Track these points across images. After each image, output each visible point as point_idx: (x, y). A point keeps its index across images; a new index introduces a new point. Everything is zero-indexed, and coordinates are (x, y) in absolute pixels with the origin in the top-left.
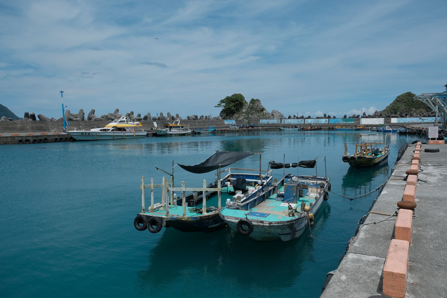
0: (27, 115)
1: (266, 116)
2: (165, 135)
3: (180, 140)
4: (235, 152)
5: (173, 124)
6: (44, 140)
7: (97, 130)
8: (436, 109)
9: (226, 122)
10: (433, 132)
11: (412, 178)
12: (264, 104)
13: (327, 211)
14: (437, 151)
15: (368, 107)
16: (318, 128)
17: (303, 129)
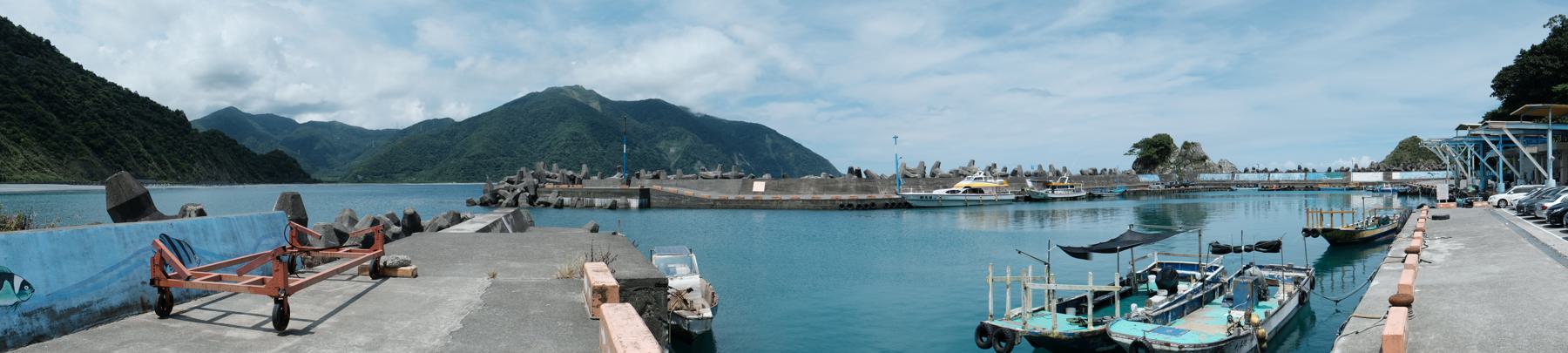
0: (851, 170)
1: (1208, 169)
2: (1045, 200)
3: (1068, 206)
4: (1157, 225)
5: (1058, 183)
6: (870, 206)
7: (942, 192)
8: (1446, 161)
9: (1144, 178)
10: (1443, 192)
11: (1412, 258)
12: (1206, 150)
13: (1308, 321)
14: (1446, 217)
15: (1363, 154)
16: (1290, 187)
17: (1266, 188)
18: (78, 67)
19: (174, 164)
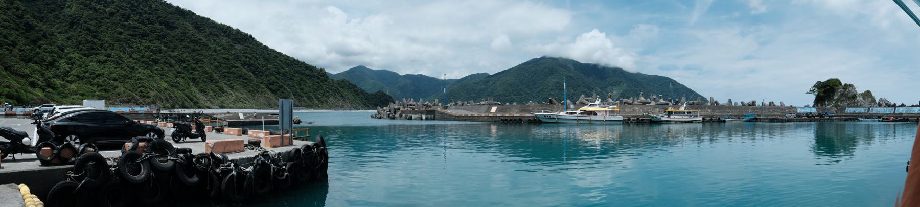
18: (266, 47)
19: (317, 98)
